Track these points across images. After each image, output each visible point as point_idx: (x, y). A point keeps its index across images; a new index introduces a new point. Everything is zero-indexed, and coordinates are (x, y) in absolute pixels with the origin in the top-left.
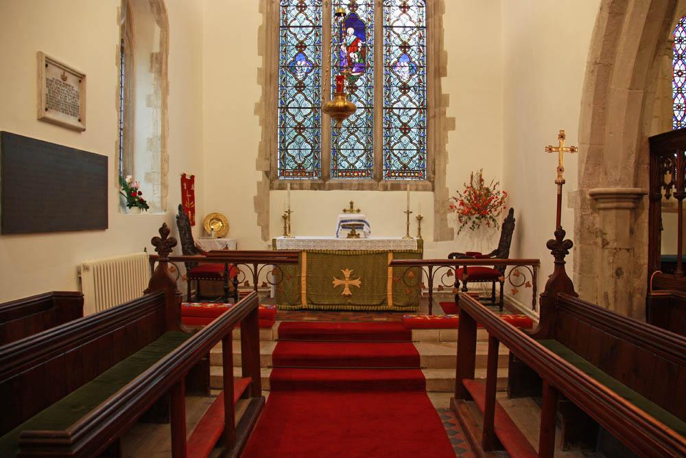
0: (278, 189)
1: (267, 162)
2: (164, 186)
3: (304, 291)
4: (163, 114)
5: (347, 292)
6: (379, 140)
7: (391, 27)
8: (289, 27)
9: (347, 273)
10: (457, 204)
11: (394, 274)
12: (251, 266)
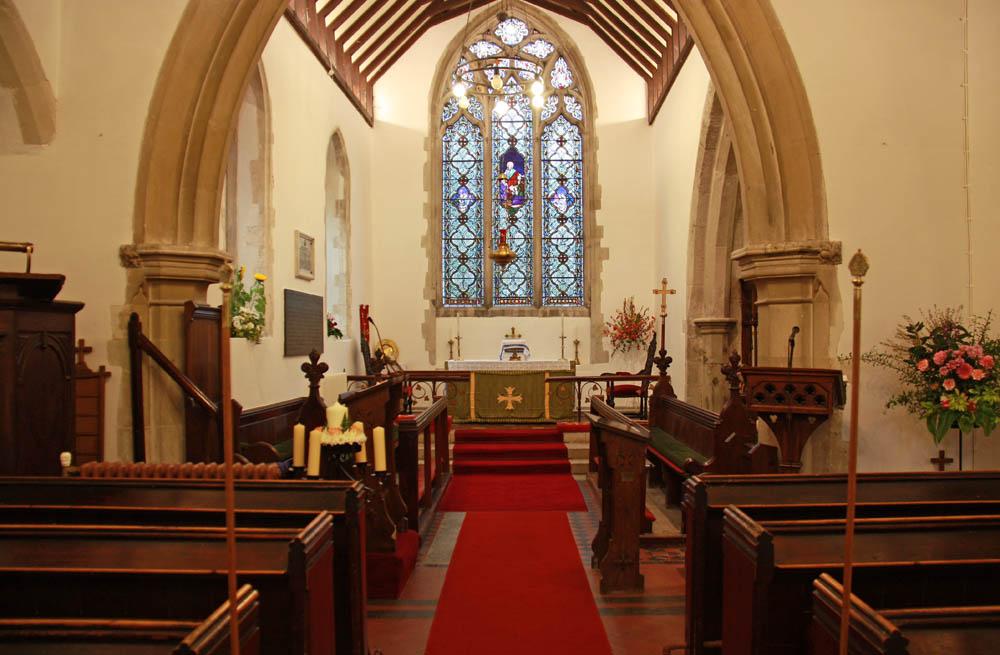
0: (443, 316)
1: (434, 292)
2: (349, 316)
3: (472, 407)
4: (348, 253)
5: (510, 407)
6: (538, 269)
7: (549, 161)
8: (452, 161)
9: (510, 390)
10: (611, 329)
11: (550, 389)
12: (431, 383)
